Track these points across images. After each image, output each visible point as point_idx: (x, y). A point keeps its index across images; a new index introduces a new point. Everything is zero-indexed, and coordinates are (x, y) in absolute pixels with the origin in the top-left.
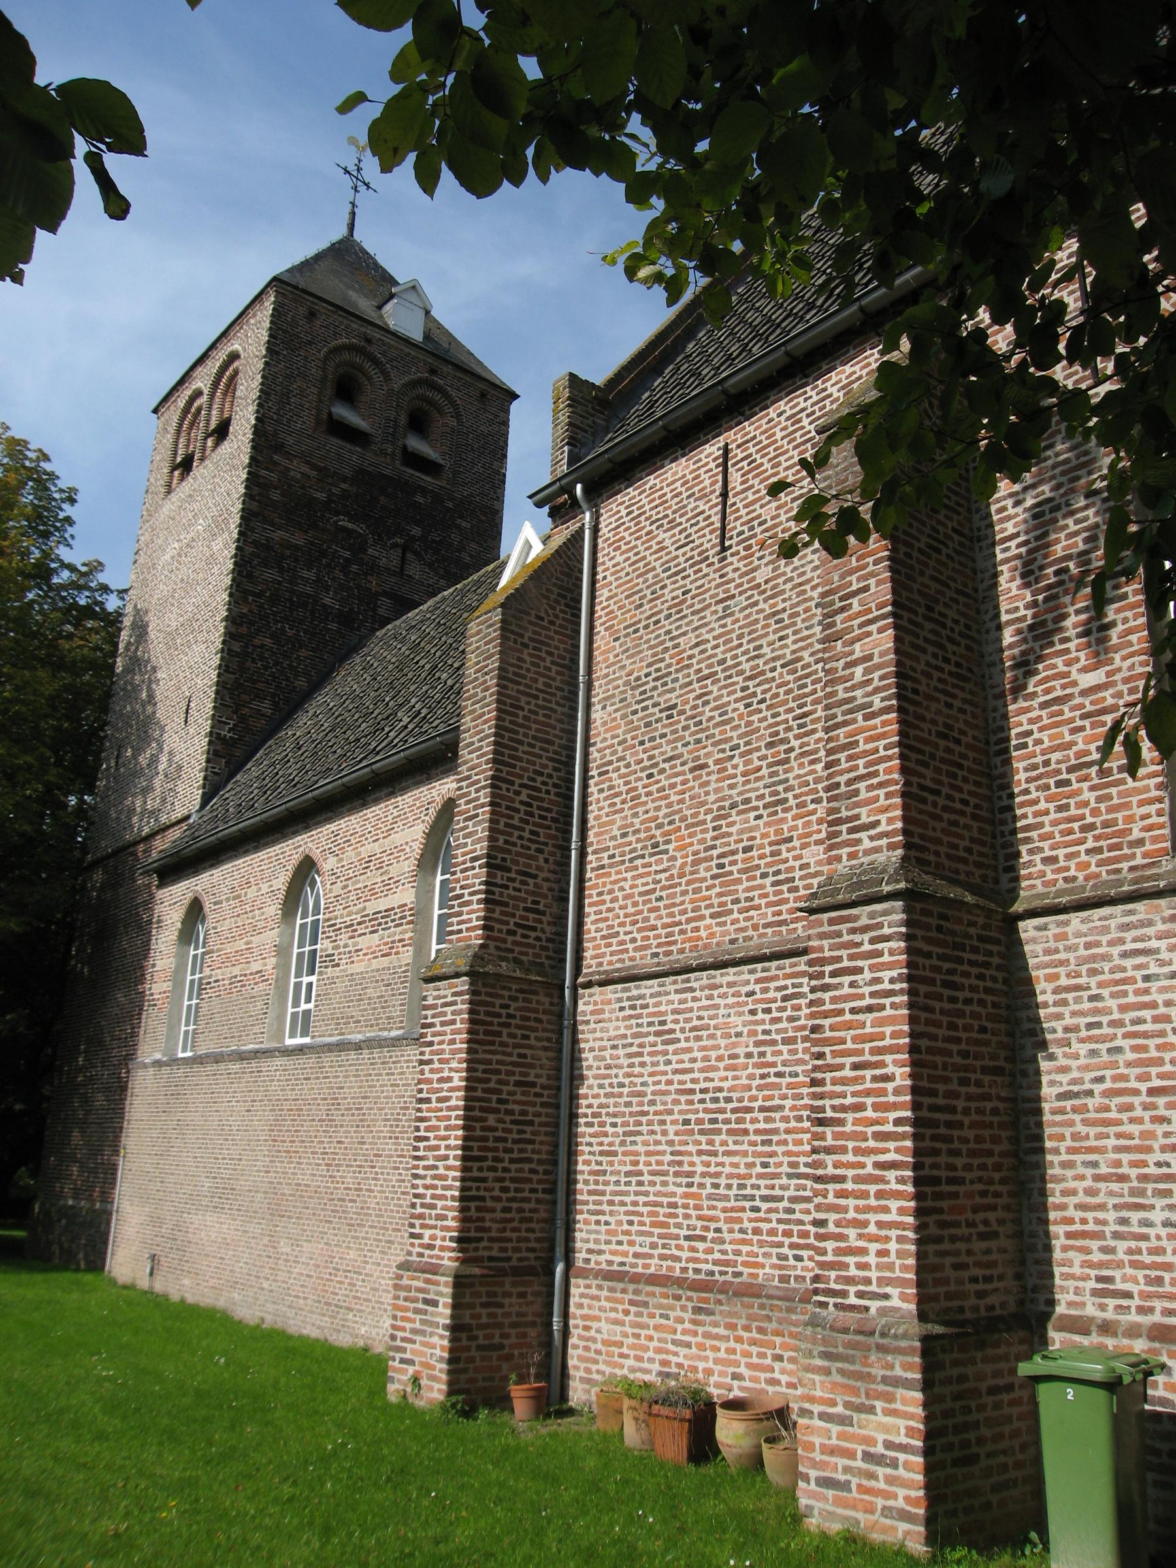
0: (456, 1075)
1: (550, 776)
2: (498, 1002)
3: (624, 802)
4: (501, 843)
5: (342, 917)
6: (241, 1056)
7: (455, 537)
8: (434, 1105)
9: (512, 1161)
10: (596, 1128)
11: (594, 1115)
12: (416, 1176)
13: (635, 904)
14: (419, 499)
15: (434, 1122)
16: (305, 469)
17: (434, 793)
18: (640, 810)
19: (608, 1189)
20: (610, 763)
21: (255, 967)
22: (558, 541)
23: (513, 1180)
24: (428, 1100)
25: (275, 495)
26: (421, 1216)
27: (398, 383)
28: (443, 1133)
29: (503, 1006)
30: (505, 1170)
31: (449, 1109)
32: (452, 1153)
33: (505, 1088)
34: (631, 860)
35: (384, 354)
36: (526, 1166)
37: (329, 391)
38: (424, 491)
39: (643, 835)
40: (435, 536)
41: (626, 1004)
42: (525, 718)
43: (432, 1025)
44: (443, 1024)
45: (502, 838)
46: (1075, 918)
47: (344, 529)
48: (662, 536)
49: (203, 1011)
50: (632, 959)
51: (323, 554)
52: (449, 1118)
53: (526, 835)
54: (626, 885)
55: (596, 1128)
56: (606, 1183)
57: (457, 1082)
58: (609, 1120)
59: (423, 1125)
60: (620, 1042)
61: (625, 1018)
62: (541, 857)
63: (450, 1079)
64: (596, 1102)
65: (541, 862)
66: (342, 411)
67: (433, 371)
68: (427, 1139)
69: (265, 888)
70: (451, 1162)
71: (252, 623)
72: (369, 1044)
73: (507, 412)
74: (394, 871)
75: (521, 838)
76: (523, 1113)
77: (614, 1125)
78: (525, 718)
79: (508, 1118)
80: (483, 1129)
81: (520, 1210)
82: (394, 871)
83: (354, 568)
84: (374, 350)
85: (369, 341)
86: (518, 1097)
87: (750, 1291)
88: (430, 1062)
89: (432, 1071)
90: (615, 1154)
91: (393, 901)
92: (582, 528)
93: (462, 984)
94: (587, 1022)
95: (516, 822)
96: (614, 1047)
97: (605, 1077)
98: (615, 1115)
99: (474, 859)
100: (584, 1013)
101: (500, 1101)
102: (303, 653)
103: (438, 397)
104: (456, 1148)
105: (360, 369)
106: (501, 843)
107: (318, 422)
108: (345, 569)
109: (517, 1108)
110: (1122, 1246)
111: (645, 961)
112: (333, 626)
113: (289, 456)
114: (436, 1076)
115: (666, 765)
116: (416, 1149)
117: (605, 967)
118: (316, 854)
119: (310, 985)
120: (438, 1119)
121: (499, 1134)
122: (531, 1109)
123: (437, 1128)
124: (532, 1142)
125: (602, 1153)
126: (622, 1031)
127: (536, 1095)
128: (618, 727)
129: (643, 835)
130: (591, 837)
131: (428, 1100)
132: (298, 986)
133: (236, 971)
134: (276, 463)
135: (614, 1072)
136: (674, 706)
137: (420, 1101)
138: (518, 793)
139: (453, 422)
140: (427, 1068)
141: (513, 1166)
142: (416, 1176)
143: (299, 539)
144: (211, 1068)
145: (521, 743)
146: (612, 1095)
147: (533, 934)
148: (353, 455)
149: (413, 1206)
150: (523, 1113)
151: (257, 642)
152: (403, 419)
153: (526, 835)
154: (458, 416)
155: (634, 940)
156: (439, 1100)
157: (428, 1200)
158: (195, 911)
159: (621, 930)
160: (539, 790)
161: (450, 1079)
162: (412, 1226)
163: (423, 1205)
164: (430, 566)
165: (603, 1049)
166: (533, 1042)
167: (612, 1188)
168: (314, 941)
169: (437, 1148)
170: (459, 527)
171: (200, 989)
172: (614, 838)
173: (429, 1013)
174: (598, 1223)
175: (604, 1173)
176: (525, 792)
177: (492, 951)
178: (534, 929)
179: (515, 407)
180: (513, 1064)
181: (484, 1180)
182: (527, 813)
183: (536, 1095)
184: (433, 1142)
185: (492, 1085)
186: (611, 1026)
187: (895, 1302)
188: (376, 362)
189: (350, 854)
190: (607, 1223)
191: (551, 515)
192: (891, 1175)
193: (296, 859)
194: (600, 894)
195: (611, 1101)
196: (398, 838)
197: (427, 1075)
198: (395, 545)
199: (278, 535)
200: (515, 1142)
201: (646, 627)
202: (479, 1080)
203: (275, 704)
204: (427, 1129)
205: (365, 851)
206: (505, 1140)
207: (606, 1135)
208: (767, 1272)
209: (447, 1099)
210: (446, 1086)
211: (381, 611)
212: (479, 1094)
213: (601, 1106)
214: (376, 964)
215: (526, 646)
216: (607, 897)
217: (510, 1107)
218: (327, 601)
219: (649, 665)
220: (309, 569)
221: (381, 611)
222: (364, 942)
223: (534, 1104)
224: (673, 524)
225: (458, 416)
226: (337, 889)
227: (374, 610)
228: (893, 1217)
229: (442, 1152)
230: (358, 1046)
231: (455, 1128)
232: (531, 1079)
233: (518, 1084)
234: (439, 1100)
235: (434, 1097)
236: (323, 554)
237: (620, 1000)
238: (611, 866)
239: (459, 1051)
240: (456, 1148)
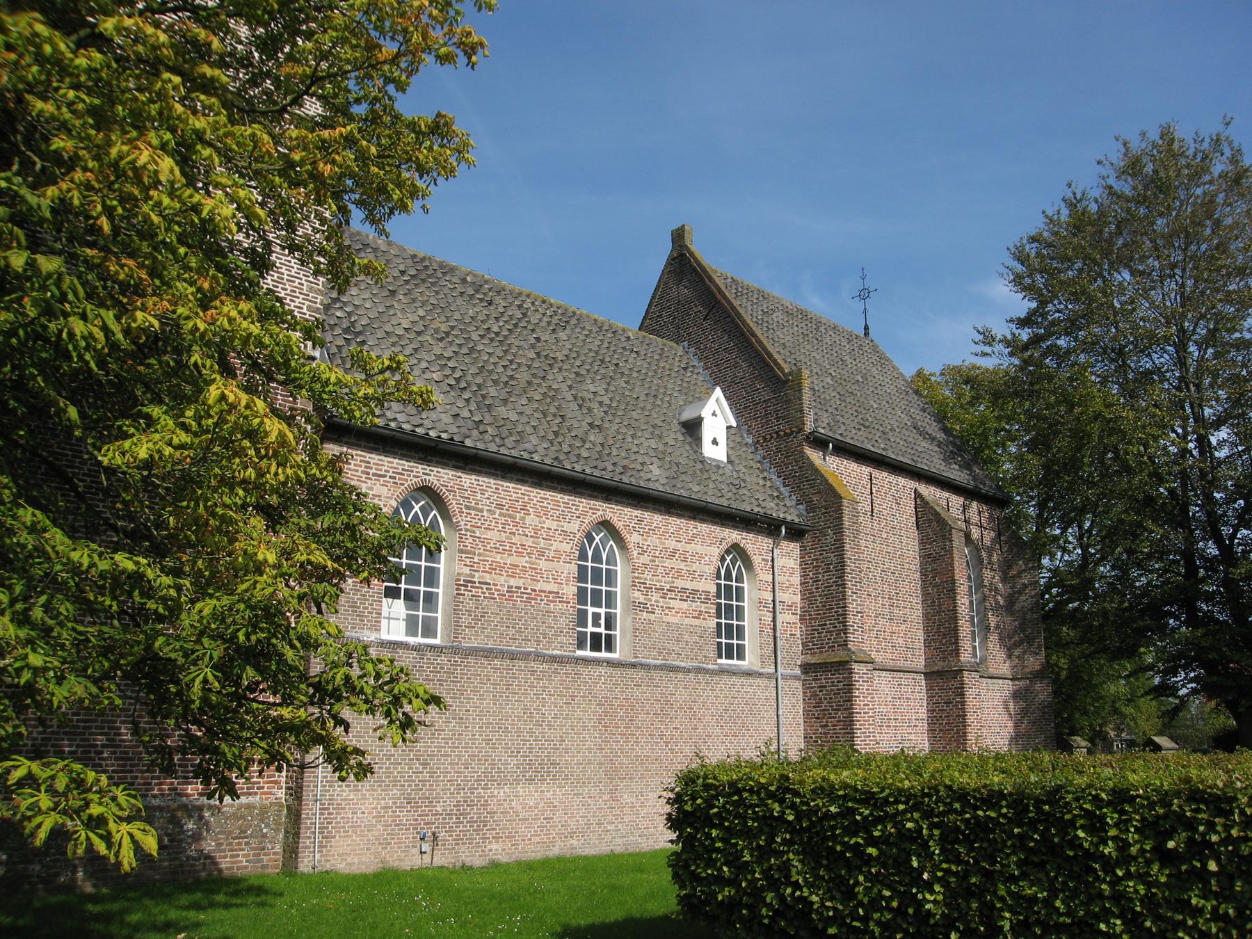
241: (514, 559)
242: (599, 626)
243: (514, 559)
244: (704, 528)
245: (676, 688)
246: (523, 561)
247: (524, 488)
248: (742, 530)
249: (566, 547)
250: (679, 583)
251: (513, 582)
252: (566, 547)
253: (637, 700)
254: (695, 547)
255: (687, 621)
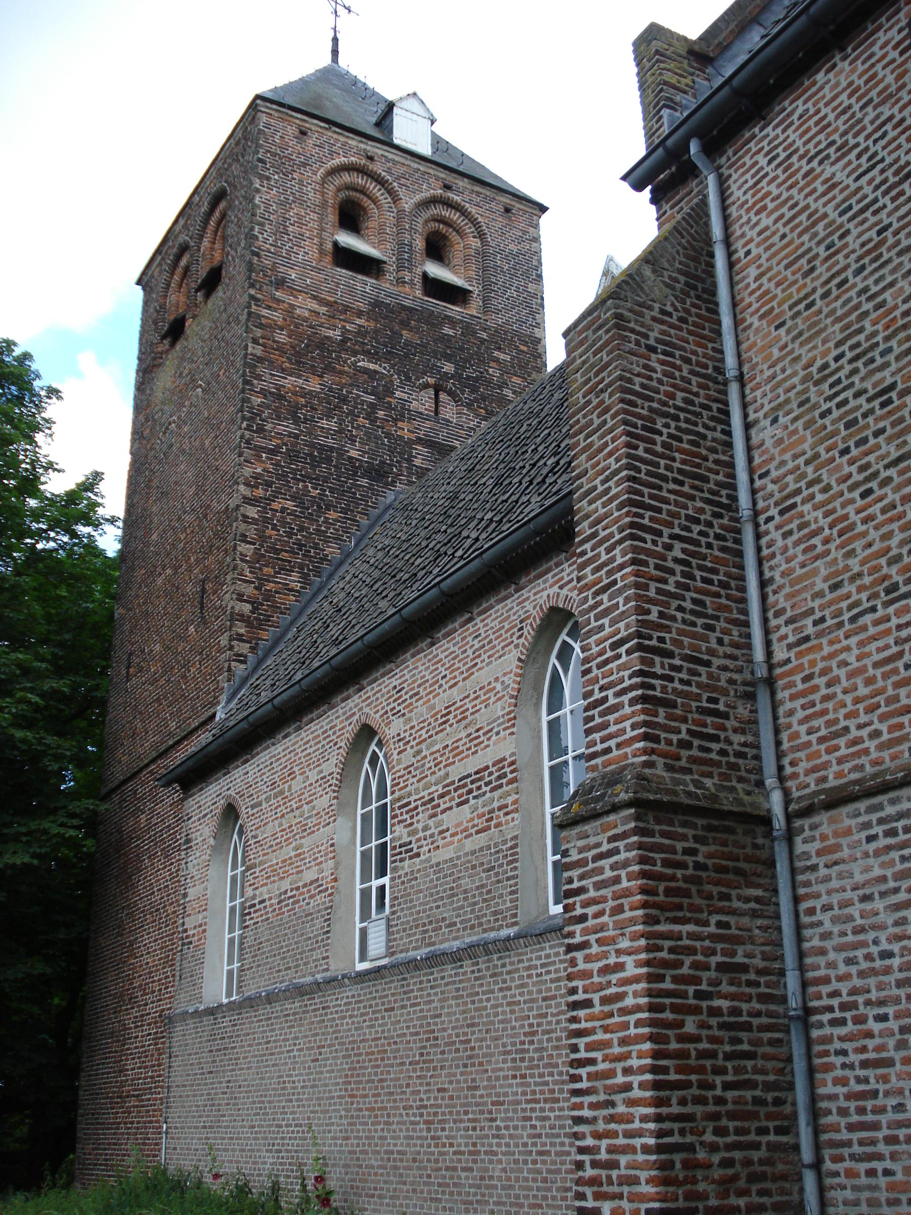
0: (629, 960)
1: (710, 524)
2: (680, 846)
3: (826, 541)
4: (654, 616)
5: (416, 791)
6: (300, 991)
7: (494, 372)
8: (597, 1009)
9: (727, 1086)
10: (850, 1027)
11: (844, 1007)
12: (578, 1120)
13: (869, 681)
14: (447, 331)
15: (600, 1036)
16: (315, 306)
17: (528, 606)
18: (858, 545)
19: (884, 1119)
20: (798, 492)
21: (309, 876)
22: (676, 216)
23: (732, 1116)
24: (588, 1004)
25: (282, 337)
26: (594, 1182)
27: (408, 202)
28: (616, 1050)
29: (688, 852)
30: (720, 1101)
31: (624, 1011)
32: (636, 1080)
33: (705, 975)
34: (853, 620)
35: (389, 171)
36: (748, 1094)
37: (332, 217)
38: (452, 322)
39: (867, 580)
40: (470, 372)
41: (879, 830)
42: (664, 445)
43: (582, 890)
44: (598, 886)
45: (655, 610)
47: (366, 371)
48: (829, 171)
49: (249, 941)
50: (875, 763)
51: (344, 400)
52: (625, 1026)
53: (688, 605)
54: (852, 658)
55: (850, 1027)
56: (882, 1110)
57: (631, 970)
58: (872, 1012)
59: (582, 1042)
60: (876, 890)
61: (877, 853)
62: (713, 637)
63: (620, 967)
64: (844, 988)
65: (714, 645)
66: (346, 239)
67: (447, 187)
68: (592, 1062)
69: (313, 776)
70: (636, 1093)
71: (268, 484)
72: (470, 952)
73: (537, 226)
74: (482, 719)
75: (680, 609)
76: (735, 1012)
77: (883, 1018)
78: (664, 445)
79: (714, 1021)
80: (681, 1039)
81: (748, 1162)
82: (482, 719)
83: (381, 414)
84: (378, 168)
85: (371, 158)
86: (725, 988)
88: (584, 945)
89: (588, 959)
90: (890, 1063)
92: (704, 202)
93: (623, 821)
94: (814, 868)
95: (671, 588)
96: (866, 898)
97: (855, 946)
98: (881, 1003)
99: (615, 646)
100: (806, 855)
101: (699, 995)
102: (332, 515)
103: (454, 216)
104: (642, 1070)
105: (363, 191)
106: (654, 616)
107: (322, 252)
108: (371, 416)
109: (724, 1004)
112: (364, 482)
113: (293, 291)
114: (596, 966)
115: (892, 472)
116: (576, 1078)
117: (832, 783)
118: (375, 720)
119: (382, 889)
120: (606, 1029)
121: (704, 1045)
122: (744, 1006)
123: (607, 1044)
124: (751, 1056)
125: (865, 1064)
126: (877, 872)
127: (749, 983)
128: (803, 440)
129: (867, 580)
130: (779, 600)
131: (588, 1004)
132: (365, 894)
133: (286, 885)
134: (278, 301)
135: (871, 935)
136: (892, 387)
137: (575, 1006)
138: (669, 547)
139: (475, 243)
140: (579, 955)
141: (730, 1095)
142: (578, 1120)
143: (314, 385)
144: (263, 1011)
145: (665, 479)
146: (873, 972)
147: (715, 746)
148: (365, 284)
149: (580, 1165)
150: (735, 1012)
151: (275, 506)
152: (420, 244)
153: (688, 605)
154: (481, 235)
155: (877, 734)
156: (605, 1001)
157: (603, 1156)
158: (231, 813)
159: (852, 724)
160: (697, 544)
161: (620, 967)
162: (581, 1196)
163: (595, 1164)
164: (469, 406)
165: (848, 904)
166: (736, 904)
167: (890, 1116)
168: (382, 832)
169: (611, 1074)
170: (497, 360)
171: (243, 915)
172: (820, 594)
173: (575, 873)
174: (871, 1173)
175: (875, 1094)
176: (678, 546)
177: (660, 771)
178: (715, 738)
179: (545, 221)
180: (712, 937)
181: (689, 1118)
182: (684, 574)
183: (749, 983)
184: (602, 1066)
185: (685, 970)
186: (856, 868)
189: (421, 709)
190: (887, 1172)
191: (654, 201)
193: (350, 731)
194: (807, 679)
195: (872, 981)
196: (482, 676)
197: (582, 966)
198: (426, 386)
199: (290, 382)
200: (728, 1057)
201: (824, 296)
202: (665, 964)
203: (305, 576)
204: (590, 1047)
205: (439, 703)
206: (713, 1055)
207: (869, 1035)
209: (620, 997)
210: (614, 978)
211: (418, 462)
212: (668, 985)
213: (853, 992)
214: (469, 845)
215: (653, 350)
216: (821, 681)
217: (716, 1003)
218: (354, 454)
219: (839, 344)
220: (329, 417)
221: (418, 462)
222: (449, 819)
223: (749, 999)
224: (844, 150)
225: (481, 235)
226: (408, 758)
227: (409, 461)
229: (620, 1079)
230: (456, 957)
231: (638, 1039)
232: (739, 959)
233: (721, 967)
234: (605, 1001)
235: (596, 998)
236: (344, 400)
237: (867, 825)
238: (819, 635)
239: (633, 921)
240: (642, 1070)
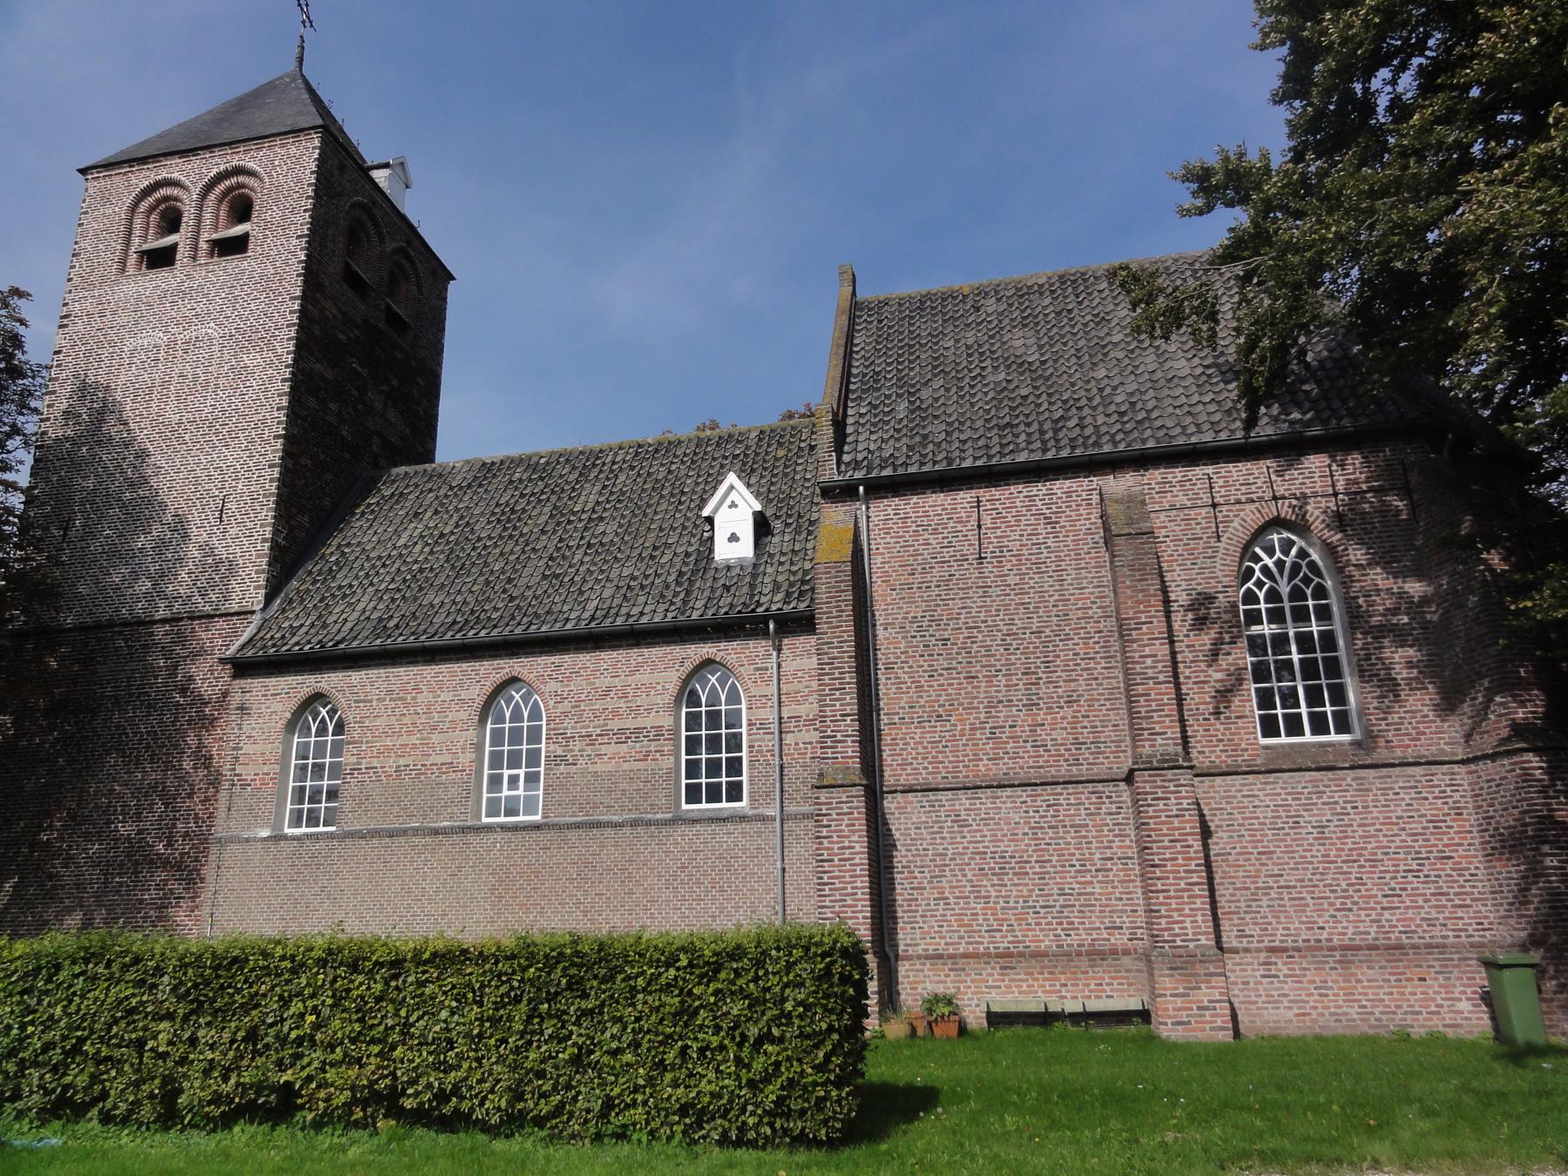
16: (334, 311)
27: (389, 247)
46: (1218, 780)
85: (374, 203)
87: (1038, 955)
91: (649, 721)
110: (1248, 917)
111: (937, 780)
139: (414, 289)
143: (329, 375)
154: (419, 287)
179: (452, 285)
187: (1204, 942)
188: (376, 224)
192: (1196, 888)
199: (318, 367)
208: (1046, 943)
214: (626, 766)
218: (345, 433)
225: (419, 287)
228: (1198, 905)
241: (404, 739)
242: (1268, 680)
243: (404, 739)
244: (655, 653)
245: (602, 846)
246: (414, 740)
247: (415, 669)
248: (719, 639)
249: (463, 715)
250: (615, 725)
251: (402, 762)
252: (463, 715)
253: (544, 866)
254: (644, 677)
255: (626, 766)
